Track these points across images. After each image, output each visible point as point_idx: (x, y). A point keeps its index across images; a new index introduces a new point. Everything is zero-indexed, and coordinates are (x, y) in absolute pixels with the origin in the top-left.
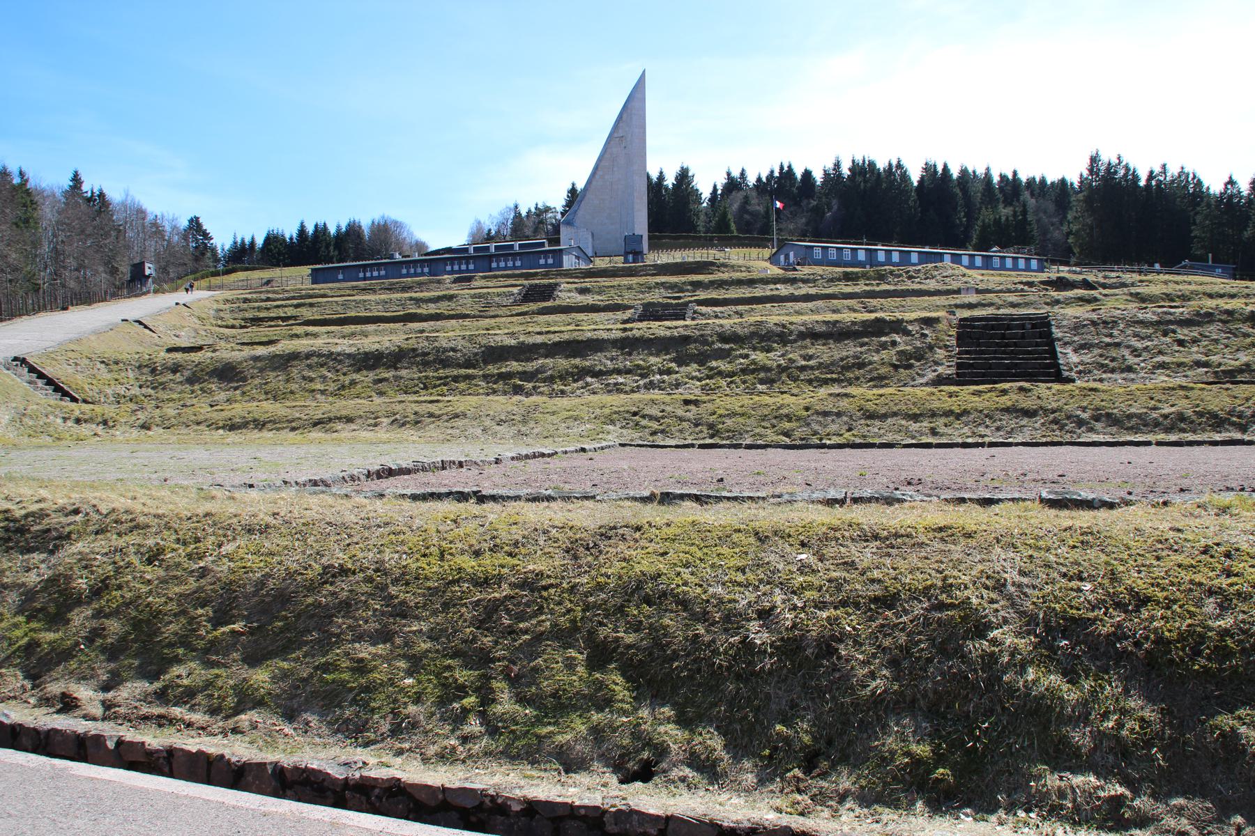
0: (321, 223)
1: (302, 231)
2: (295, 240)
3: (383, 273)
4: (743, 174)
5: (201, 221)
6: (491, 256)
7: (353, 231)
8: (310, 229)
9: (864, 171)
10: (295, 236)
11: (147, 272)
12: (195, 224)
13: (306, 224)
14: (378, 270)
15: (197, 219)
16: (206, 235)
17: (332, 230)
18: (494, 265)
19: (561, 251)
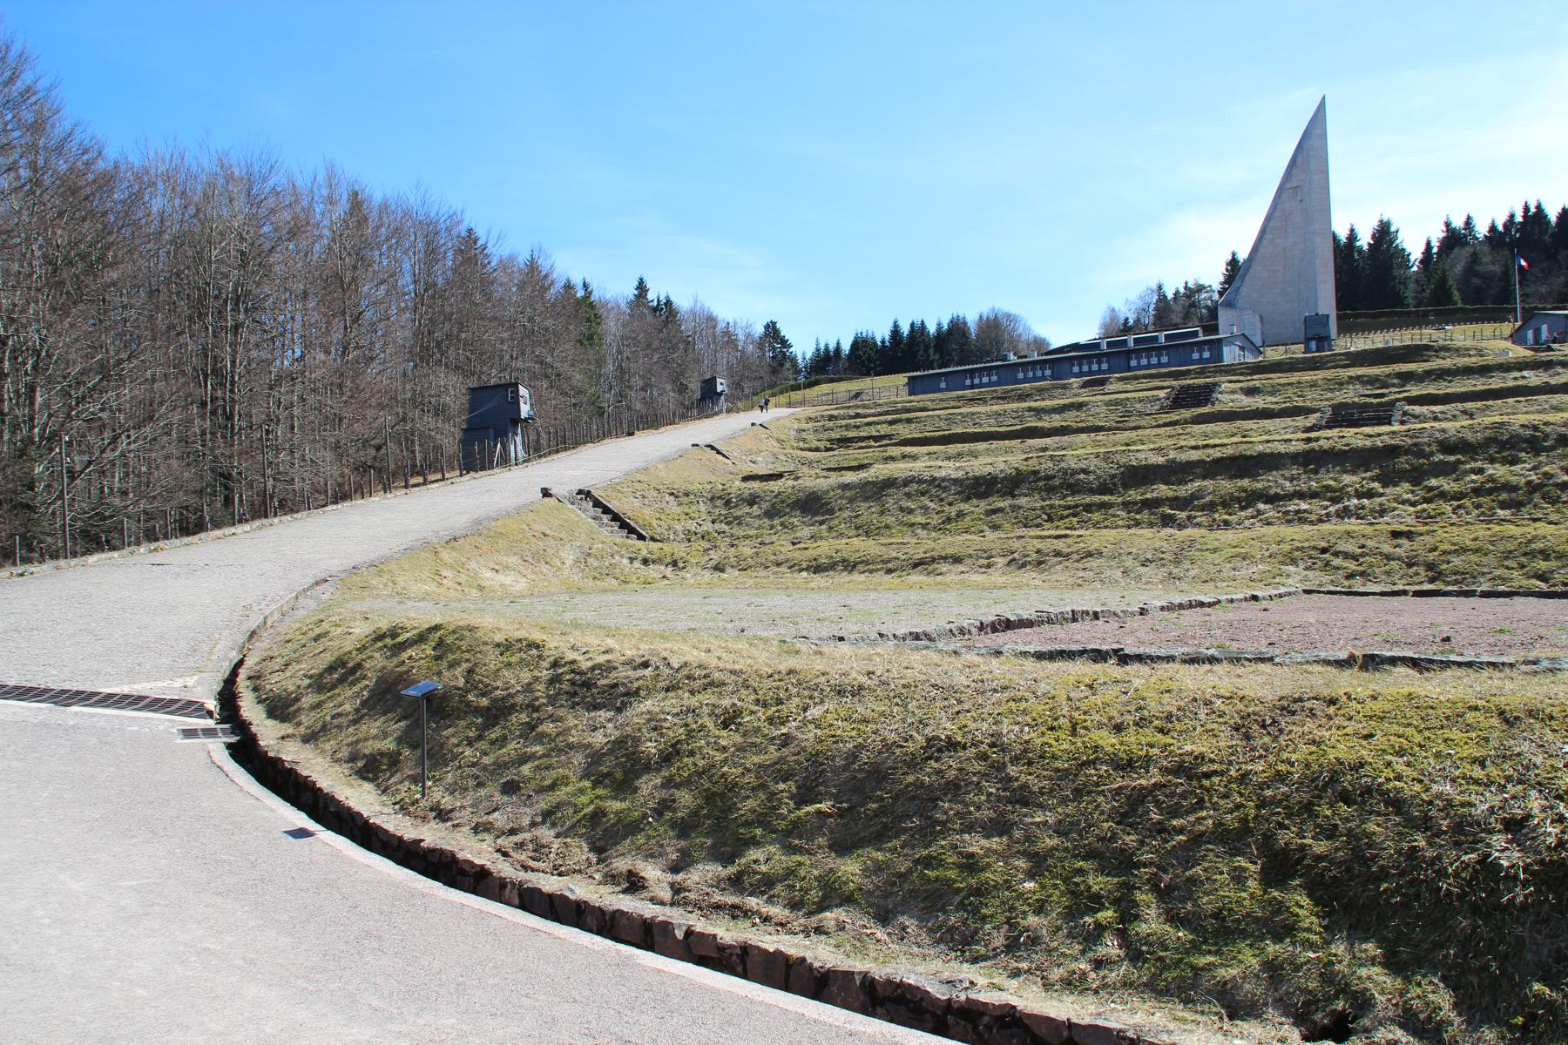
0: (918, 322)
1: (896, 332)
3: (994, 378)
5: (778, 326)
6: (1130, 352)
7: (957, 328)
10: (887, 338)
11: (719, 388)
12: (772, 330)
13: (900, 323)
14: (989, 376)
15: (774, 324)
16: (784, 343)
18: (1133, 363)
19: (1220, 340)
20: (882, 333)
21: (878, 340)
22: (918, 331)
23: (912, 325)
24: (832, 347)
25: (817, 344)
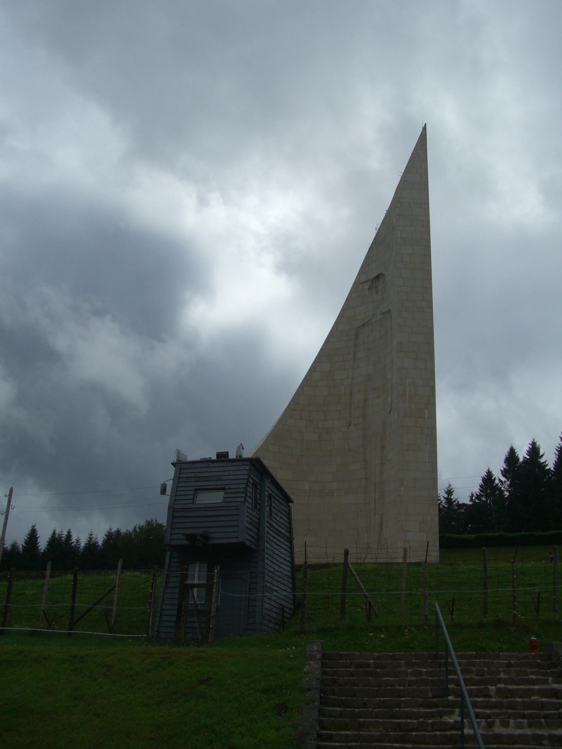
1: (33, 536)
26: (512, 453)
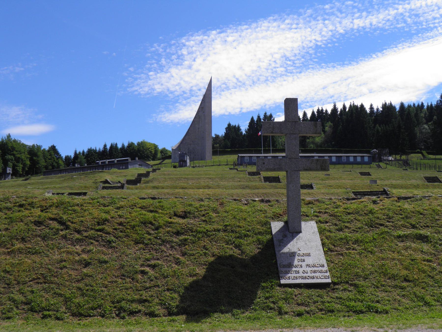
1: (105, 146)
2: (347, 110)
4: (96, 148)
6: (107, 165)
8: (406, 105)
9: (353, 108)
11: (8, 172)
17: (120, 146)
20: (99, 147)
21: (98, 149)
22: (114, 147)
23: (112, 144)
24: (429, 104)
25: (428, 104)
26: (252, 119)
